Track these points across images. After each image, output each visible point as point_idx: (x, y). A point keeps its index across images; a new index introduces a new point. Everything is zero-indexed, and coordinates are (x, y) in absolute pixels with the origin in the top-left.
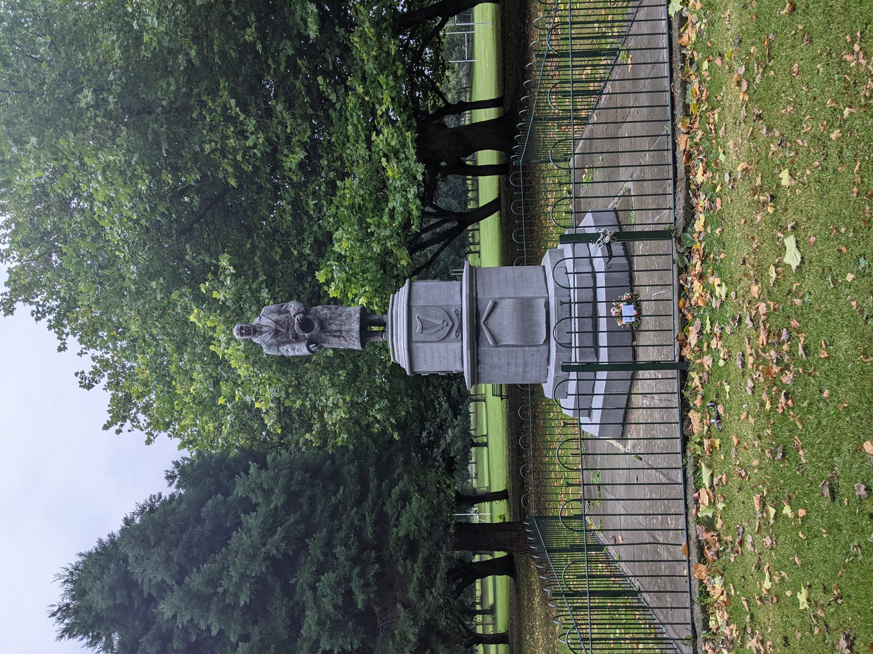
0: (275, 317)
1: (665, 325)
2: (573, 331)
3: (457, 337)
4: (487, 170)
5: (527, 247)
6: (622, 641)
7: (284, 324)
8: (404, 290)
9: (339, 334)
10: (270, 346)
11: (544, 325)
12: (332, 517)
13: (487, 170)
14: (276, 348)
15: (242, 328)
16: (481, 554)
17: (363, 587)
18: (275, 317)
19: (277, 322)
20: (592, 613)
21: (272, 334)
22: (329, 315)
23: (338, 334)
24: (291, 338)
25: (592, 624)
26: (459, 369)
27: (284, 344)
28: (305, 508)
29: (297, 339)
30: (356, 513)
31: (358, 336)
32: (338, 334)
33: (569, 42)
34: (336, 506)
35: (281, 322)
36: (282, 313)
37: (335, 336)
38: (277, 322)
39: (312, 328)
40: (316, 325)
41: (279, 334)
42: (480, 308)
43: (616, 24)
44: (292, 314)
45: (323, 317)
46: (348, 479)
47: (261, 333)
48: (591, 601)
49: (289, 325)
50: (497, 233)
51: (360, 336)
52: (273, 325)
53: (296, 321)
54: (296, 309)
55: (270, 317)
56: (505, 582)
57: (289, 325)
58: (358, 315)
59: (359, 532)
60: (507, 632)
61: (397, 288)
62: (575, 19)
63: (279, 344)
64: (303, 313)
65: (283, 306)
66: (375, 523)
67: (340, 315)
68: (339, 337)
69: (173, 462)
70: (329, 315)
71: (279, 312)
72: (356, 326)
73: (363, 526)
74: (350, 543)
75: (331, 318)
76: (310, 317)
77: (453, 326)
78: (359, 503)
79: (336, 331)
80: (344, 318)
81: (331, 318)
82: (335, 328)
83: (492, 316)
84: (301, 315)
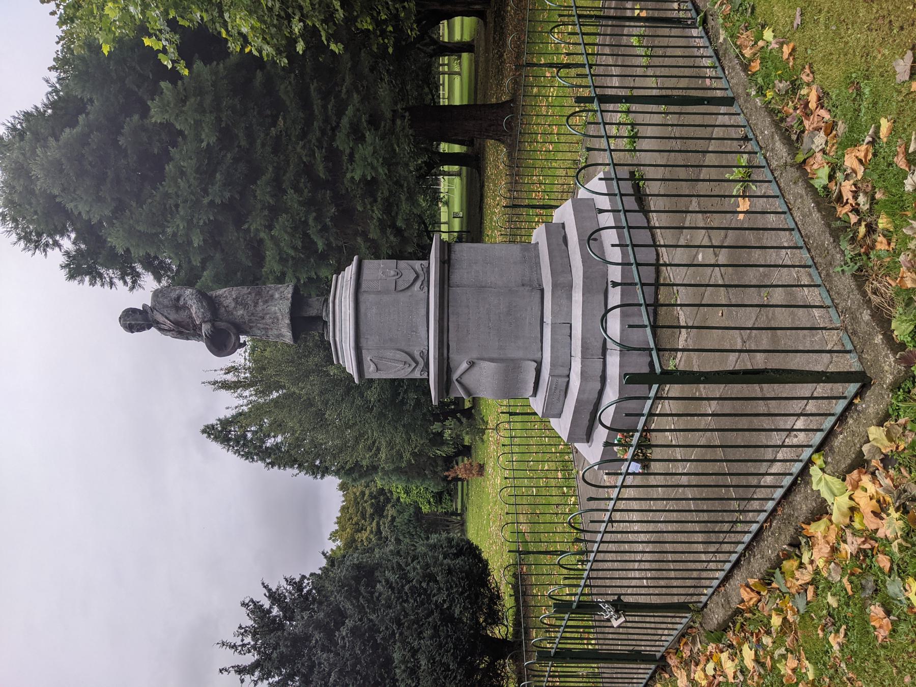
1: (674, 143)
4: (456, 49)
6: (592, 630)
8: (350, 271)
11: (532, 385)
12: (275, 151)
13: (456, 49)
16: (449, 56)
17: (321, 231)
22: (247, 318)
26: (425, 376)
28: (243, 143)
30: (304, 147)
34: (278, 137)
42: (452, 365)
43: (673, 390)
46: (288, 103)
56: (470, 60)
58: (287, 321)
59: (308, 170)
60: (473, 40)
61: (339, 270)
66: (326, 159)
69: (62, 267)
70: (247, 318)
73: (313, 162)
74: (301, 185)
76: (222, 325)
78: (304, 135)
83: (468, 372)
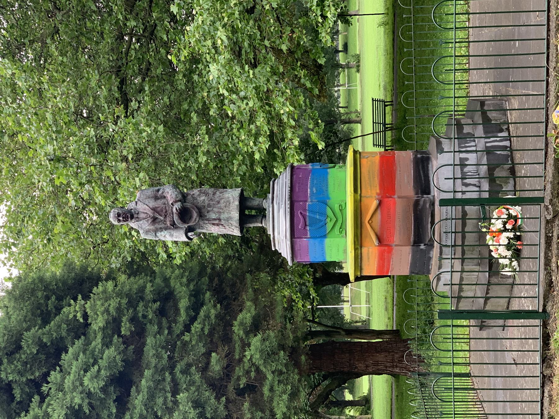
0: (152, 204)
2: (453, 234)
3: (341, 232)
5: (416, 21)
7: (162, 211)
9: (218, 222)
10: (147, 232)
14: (154, 234)
15: (119, 215)
18: (152, 204)
19: (154, 209)
20: (455, 394)
21: (150, 221)
22: (207, 202)
23: (217, 222)
24: (169, 225)
25: (455, 414)
27: (161, 229)
29: (174, 226)
31: (238, 225)
32: (217, 222)
33: (450, 354)
35: (159, 209)
36: (158, 199)
37: (214, 224)
38: (154, 209)
39: (191, 217)
40: (195, 215)
41: (157, 221)
44: (171, 202)
45: (200, 204)
47: (138, 219)
48: (455, 394)
49: (166, 212)
50: (382, 73)
51: (240, 225)
52: (150, 213)
53: (174, 210)
54: (174, 196)
55: (147, 203)
57: (166, 212)
58: (237, 203)
62: (455, 361)
63: (156, 231)
64: (180, 201)
65: (158, 190)
67: (219, 202)
68: (218, 225)
70: (207, 202)
71: (156, 198)
72: (236, 215)
75: (209, 205)
76: (188, 205)
77: (337, 221)
79: (215, 219)
80: (222, 204)
81: (209, 205)
82: (213, 216)
83: (374, 216)
84: (179, 203)
